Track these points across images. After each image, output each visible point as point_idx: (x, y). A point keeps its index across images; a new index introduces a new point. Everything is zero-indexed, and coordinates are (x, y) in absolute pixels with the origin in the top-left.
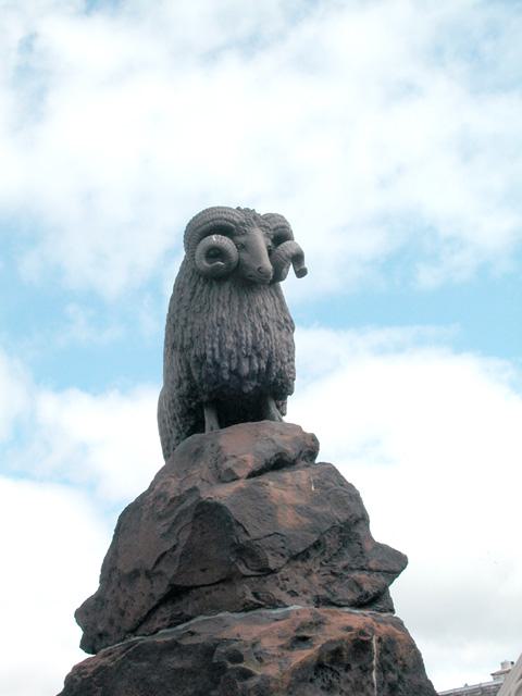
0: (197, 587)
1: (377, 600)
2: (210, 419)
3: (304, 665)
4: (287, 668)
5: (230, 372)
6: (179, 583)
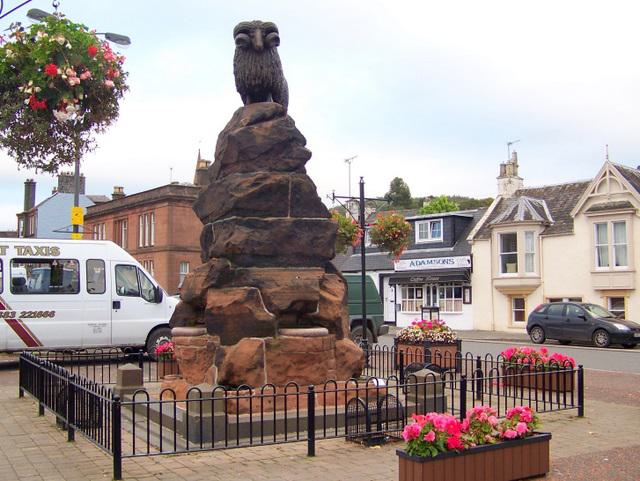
1: (300, 168)
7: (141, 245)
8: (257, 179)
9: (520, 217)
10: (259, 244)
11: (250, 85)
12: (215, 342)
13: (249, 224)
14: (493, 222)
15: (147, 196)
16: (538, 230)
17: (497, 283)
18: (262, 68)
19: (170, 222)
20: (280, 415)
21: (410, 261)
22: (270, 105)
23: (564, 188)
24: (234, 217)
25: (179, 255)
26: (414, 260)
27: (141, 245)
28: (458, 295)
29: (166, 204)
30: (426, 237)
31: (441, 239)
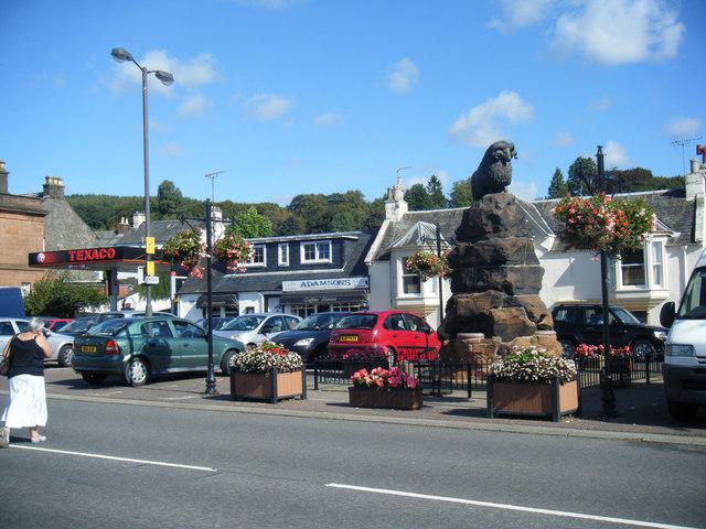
20: (222, 310)
21: (301, 282)
26: (306, 282)
30: (313, 257)
31: (330, 261)
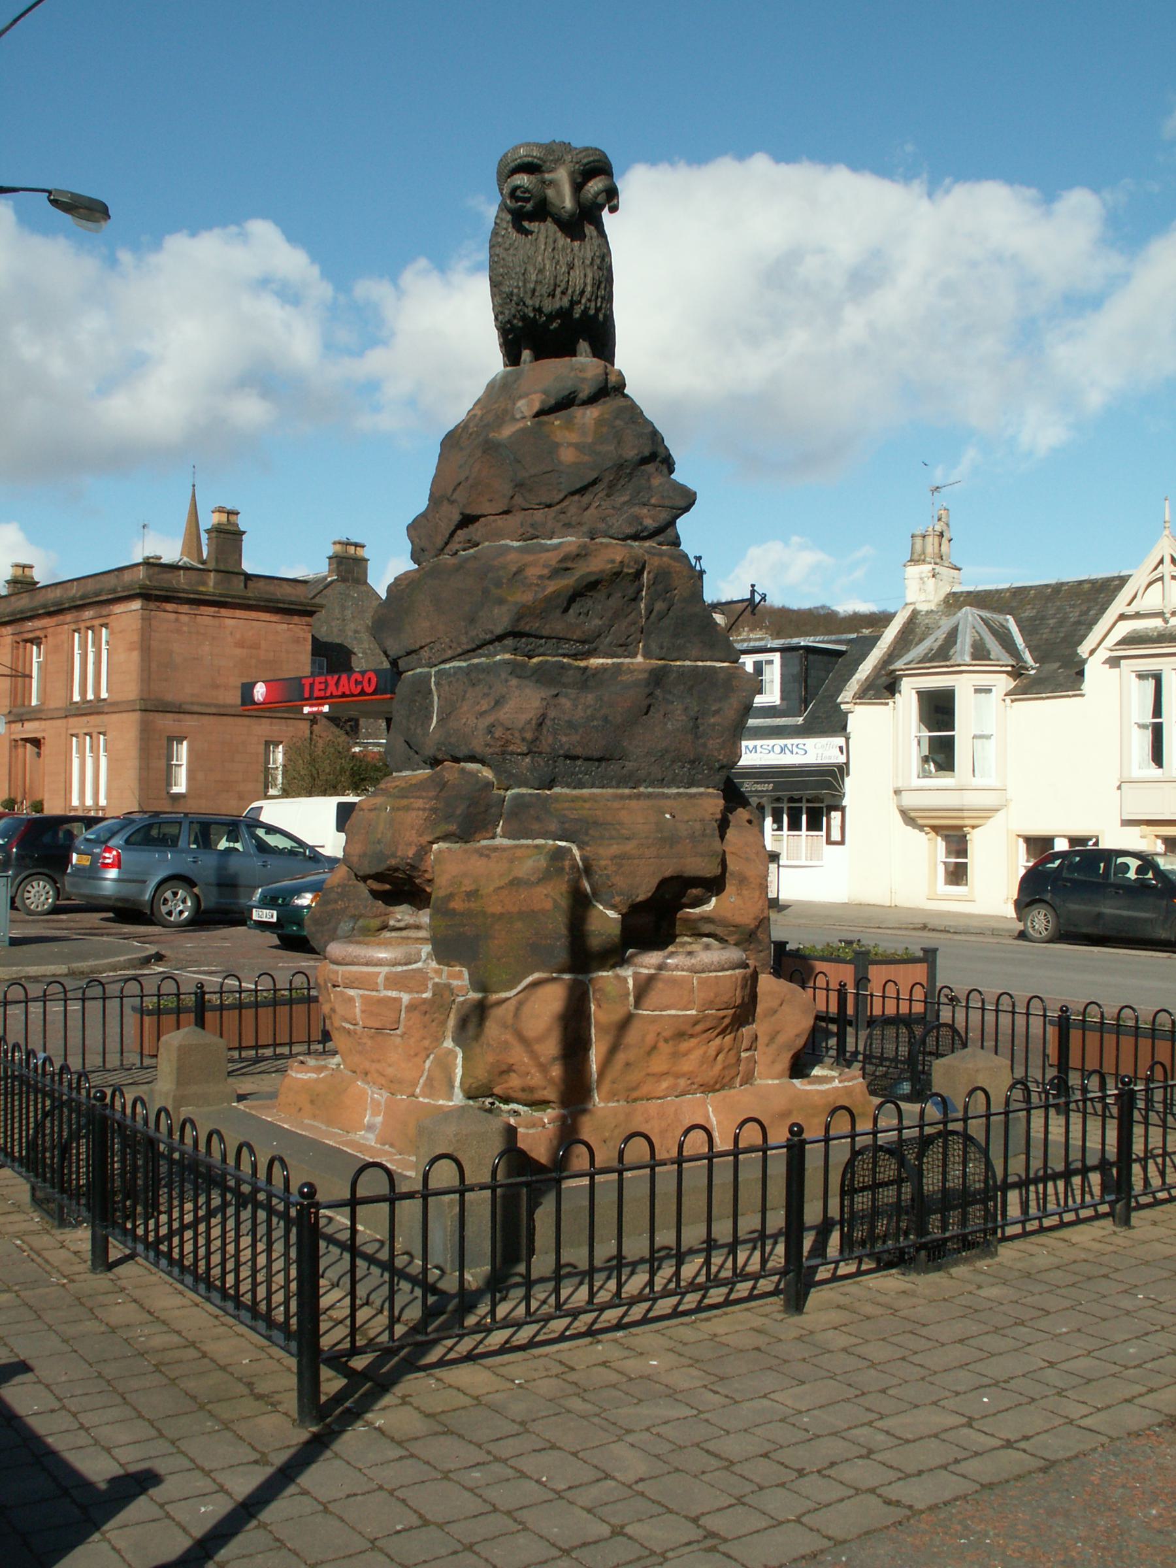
0: (485, 516)
1: (665, 531)
2: (526, 354)
3: (556, 594)
4: (541, 596)
5: (534, 310)
6: (468, 511)
7: (77, 698)
8: (564, 559)
9: (963, 650)
10: (571, 725)
11: (539, 310)
12: (455, 983)
13: (545, 677)
14: (899, 665)
15: (91, 586)
16: (1003, 683)
17: (909, 800)
18: (571, 267)
19: (146, 649)
22: (585, 362)
23: (1056, 591)
24: (507, 656)
25: (167, 723)
27: (77, 698)
28: (814, 825)
29: (136, 605)
